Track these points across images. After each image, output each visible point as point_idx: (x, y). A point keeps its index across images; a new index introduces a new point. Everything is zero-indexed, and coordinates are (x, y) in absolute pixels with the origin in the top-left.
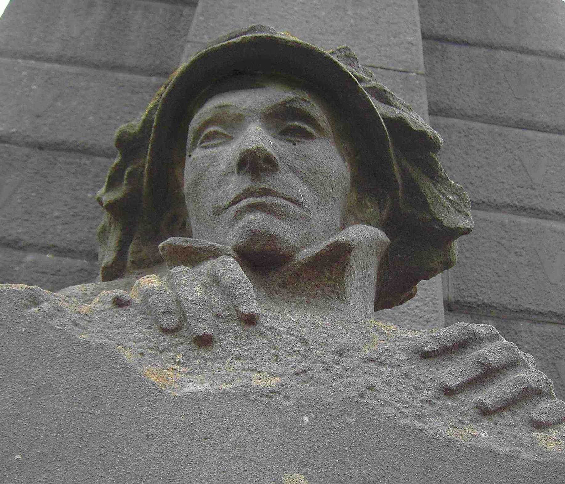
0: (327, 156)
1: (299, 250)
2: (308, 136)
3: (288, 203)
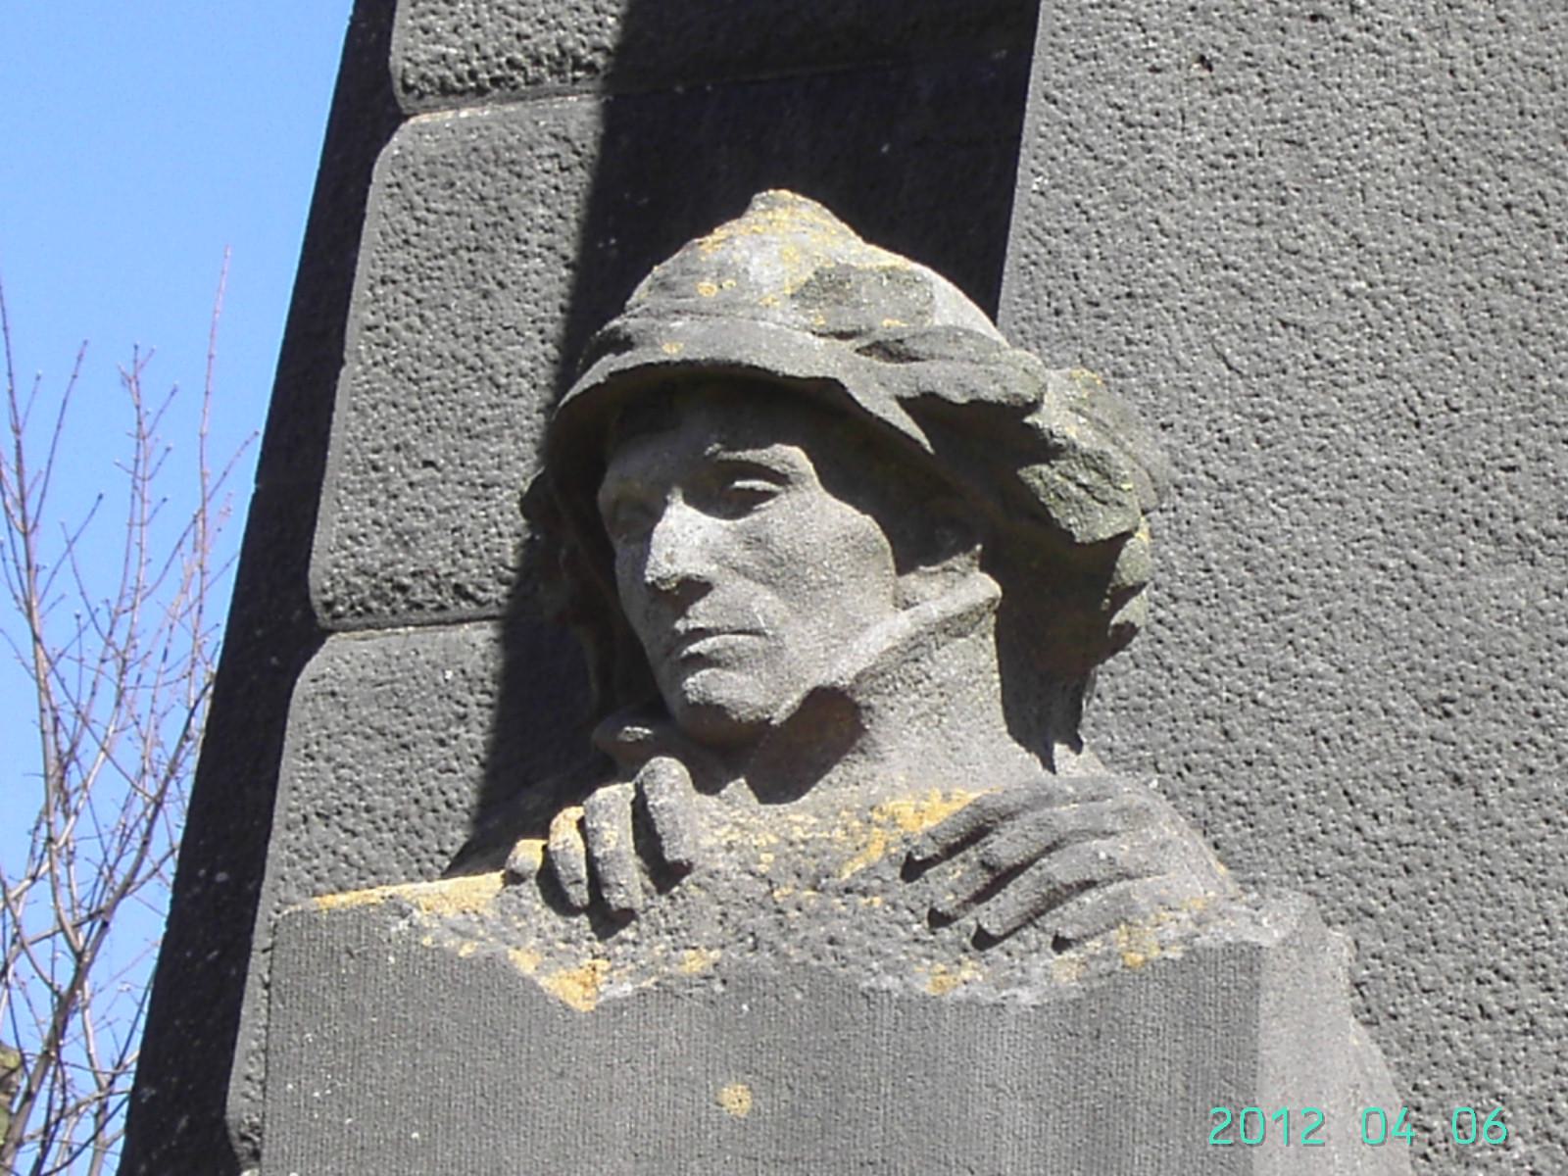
0: (814, 516)
1: (776, 707)
2: (768, 495)
3: (740, 638)
